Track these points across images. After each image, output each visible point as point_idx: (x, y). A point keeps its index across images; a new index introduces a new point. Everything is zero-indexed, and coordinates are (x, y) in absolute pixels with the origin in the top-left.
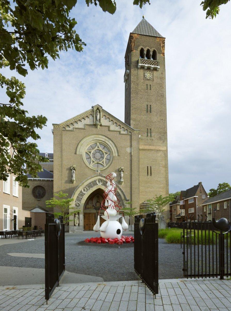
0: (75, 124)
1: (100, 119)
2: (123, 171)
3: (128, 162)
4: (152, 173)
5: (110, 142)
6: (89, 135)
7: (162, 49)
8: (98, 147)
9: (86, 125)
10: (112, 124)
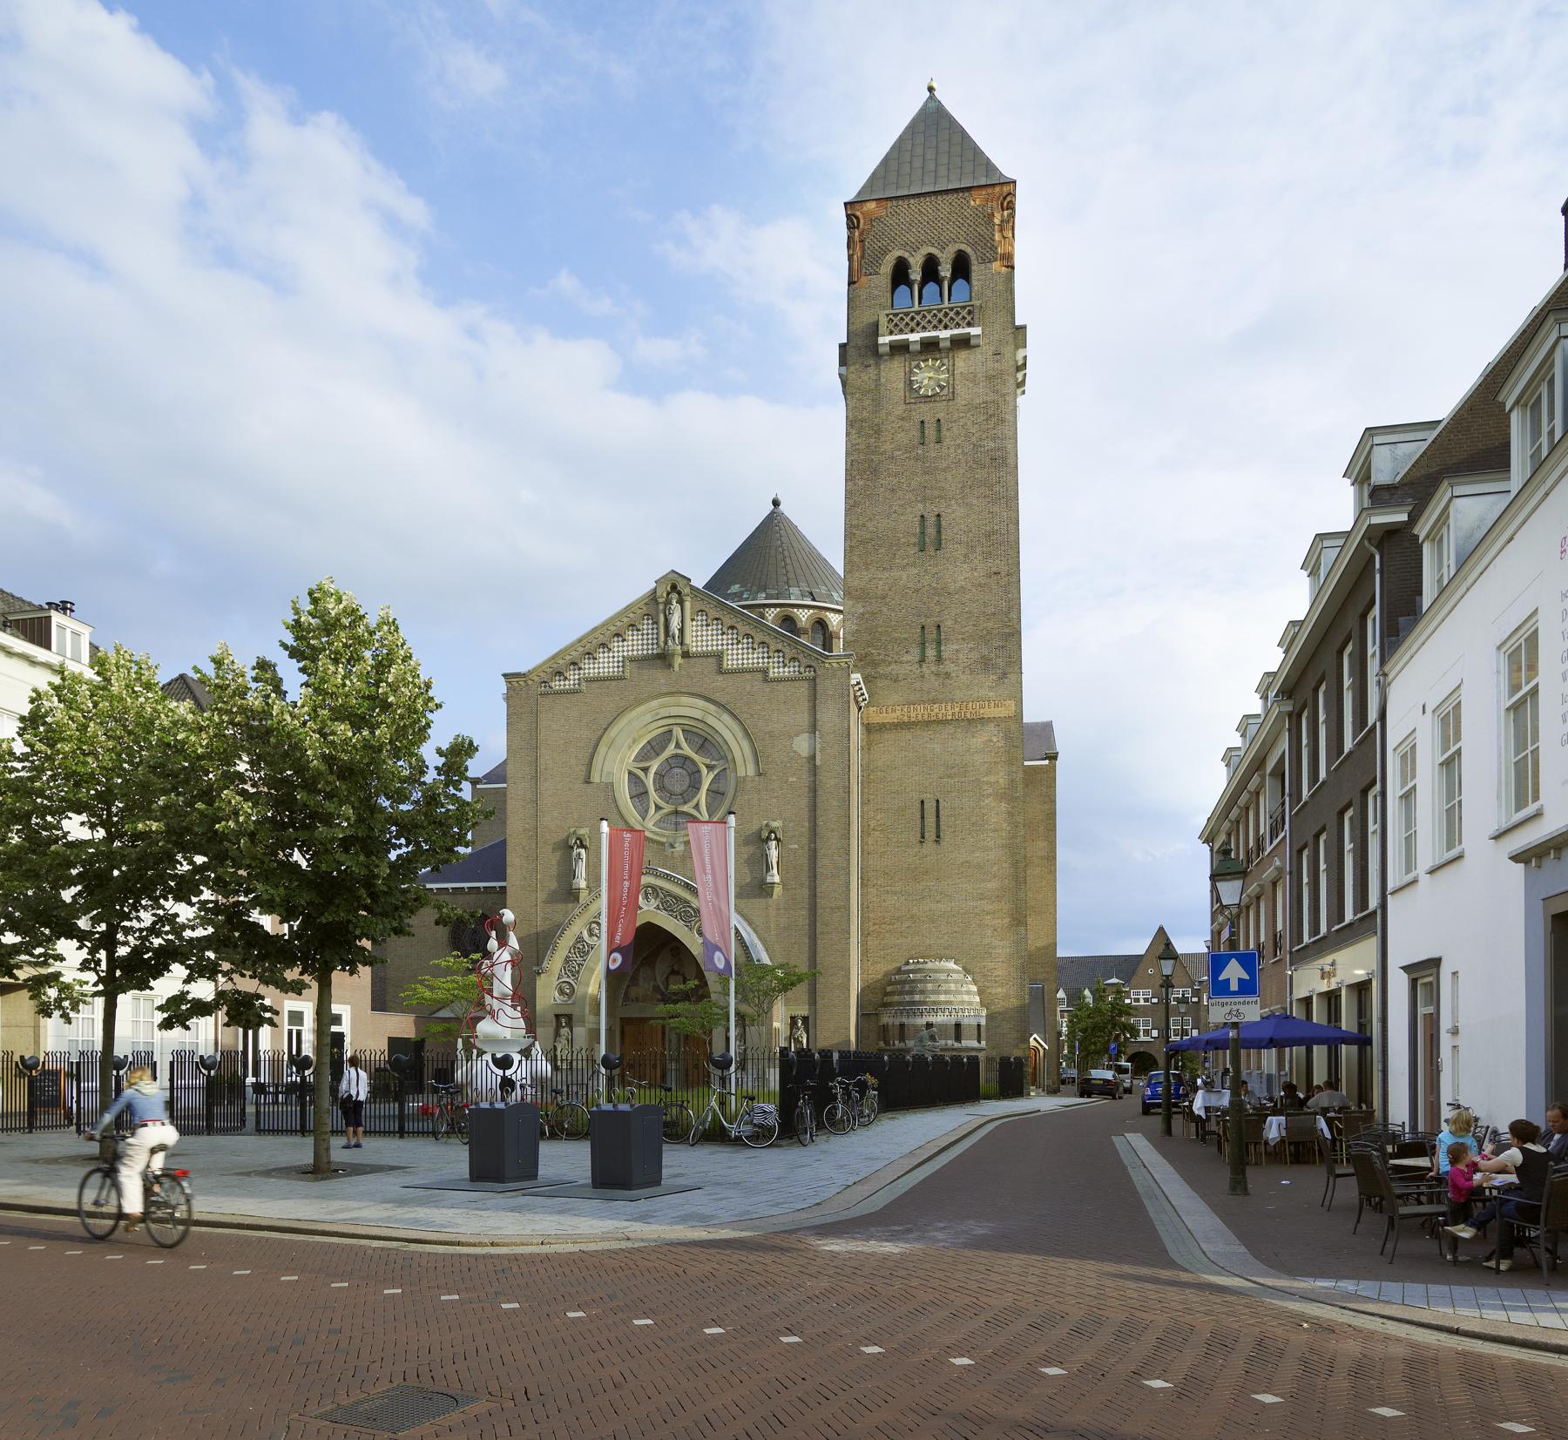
0: (586, 661)
1: (682, 631)
2: (776, 838)
3: (799, 796)
4: (942, 827)
5: (726, 717)
6: (639, 703)
7: (997, 237)
8: (678, 746)
9: (584, 684)
10: (732, 644)
